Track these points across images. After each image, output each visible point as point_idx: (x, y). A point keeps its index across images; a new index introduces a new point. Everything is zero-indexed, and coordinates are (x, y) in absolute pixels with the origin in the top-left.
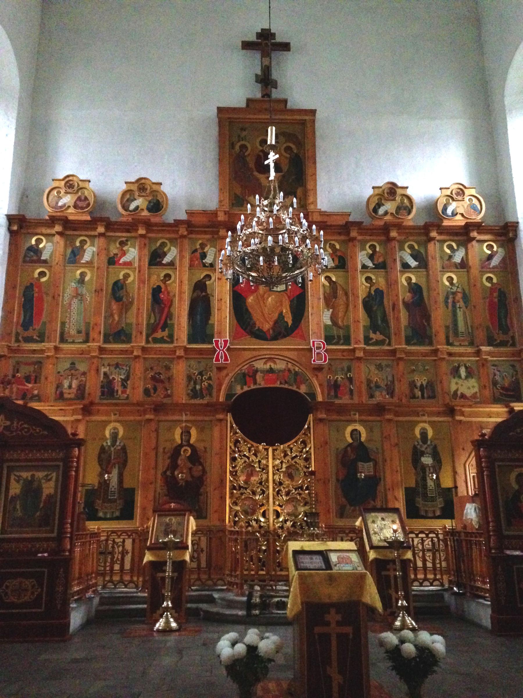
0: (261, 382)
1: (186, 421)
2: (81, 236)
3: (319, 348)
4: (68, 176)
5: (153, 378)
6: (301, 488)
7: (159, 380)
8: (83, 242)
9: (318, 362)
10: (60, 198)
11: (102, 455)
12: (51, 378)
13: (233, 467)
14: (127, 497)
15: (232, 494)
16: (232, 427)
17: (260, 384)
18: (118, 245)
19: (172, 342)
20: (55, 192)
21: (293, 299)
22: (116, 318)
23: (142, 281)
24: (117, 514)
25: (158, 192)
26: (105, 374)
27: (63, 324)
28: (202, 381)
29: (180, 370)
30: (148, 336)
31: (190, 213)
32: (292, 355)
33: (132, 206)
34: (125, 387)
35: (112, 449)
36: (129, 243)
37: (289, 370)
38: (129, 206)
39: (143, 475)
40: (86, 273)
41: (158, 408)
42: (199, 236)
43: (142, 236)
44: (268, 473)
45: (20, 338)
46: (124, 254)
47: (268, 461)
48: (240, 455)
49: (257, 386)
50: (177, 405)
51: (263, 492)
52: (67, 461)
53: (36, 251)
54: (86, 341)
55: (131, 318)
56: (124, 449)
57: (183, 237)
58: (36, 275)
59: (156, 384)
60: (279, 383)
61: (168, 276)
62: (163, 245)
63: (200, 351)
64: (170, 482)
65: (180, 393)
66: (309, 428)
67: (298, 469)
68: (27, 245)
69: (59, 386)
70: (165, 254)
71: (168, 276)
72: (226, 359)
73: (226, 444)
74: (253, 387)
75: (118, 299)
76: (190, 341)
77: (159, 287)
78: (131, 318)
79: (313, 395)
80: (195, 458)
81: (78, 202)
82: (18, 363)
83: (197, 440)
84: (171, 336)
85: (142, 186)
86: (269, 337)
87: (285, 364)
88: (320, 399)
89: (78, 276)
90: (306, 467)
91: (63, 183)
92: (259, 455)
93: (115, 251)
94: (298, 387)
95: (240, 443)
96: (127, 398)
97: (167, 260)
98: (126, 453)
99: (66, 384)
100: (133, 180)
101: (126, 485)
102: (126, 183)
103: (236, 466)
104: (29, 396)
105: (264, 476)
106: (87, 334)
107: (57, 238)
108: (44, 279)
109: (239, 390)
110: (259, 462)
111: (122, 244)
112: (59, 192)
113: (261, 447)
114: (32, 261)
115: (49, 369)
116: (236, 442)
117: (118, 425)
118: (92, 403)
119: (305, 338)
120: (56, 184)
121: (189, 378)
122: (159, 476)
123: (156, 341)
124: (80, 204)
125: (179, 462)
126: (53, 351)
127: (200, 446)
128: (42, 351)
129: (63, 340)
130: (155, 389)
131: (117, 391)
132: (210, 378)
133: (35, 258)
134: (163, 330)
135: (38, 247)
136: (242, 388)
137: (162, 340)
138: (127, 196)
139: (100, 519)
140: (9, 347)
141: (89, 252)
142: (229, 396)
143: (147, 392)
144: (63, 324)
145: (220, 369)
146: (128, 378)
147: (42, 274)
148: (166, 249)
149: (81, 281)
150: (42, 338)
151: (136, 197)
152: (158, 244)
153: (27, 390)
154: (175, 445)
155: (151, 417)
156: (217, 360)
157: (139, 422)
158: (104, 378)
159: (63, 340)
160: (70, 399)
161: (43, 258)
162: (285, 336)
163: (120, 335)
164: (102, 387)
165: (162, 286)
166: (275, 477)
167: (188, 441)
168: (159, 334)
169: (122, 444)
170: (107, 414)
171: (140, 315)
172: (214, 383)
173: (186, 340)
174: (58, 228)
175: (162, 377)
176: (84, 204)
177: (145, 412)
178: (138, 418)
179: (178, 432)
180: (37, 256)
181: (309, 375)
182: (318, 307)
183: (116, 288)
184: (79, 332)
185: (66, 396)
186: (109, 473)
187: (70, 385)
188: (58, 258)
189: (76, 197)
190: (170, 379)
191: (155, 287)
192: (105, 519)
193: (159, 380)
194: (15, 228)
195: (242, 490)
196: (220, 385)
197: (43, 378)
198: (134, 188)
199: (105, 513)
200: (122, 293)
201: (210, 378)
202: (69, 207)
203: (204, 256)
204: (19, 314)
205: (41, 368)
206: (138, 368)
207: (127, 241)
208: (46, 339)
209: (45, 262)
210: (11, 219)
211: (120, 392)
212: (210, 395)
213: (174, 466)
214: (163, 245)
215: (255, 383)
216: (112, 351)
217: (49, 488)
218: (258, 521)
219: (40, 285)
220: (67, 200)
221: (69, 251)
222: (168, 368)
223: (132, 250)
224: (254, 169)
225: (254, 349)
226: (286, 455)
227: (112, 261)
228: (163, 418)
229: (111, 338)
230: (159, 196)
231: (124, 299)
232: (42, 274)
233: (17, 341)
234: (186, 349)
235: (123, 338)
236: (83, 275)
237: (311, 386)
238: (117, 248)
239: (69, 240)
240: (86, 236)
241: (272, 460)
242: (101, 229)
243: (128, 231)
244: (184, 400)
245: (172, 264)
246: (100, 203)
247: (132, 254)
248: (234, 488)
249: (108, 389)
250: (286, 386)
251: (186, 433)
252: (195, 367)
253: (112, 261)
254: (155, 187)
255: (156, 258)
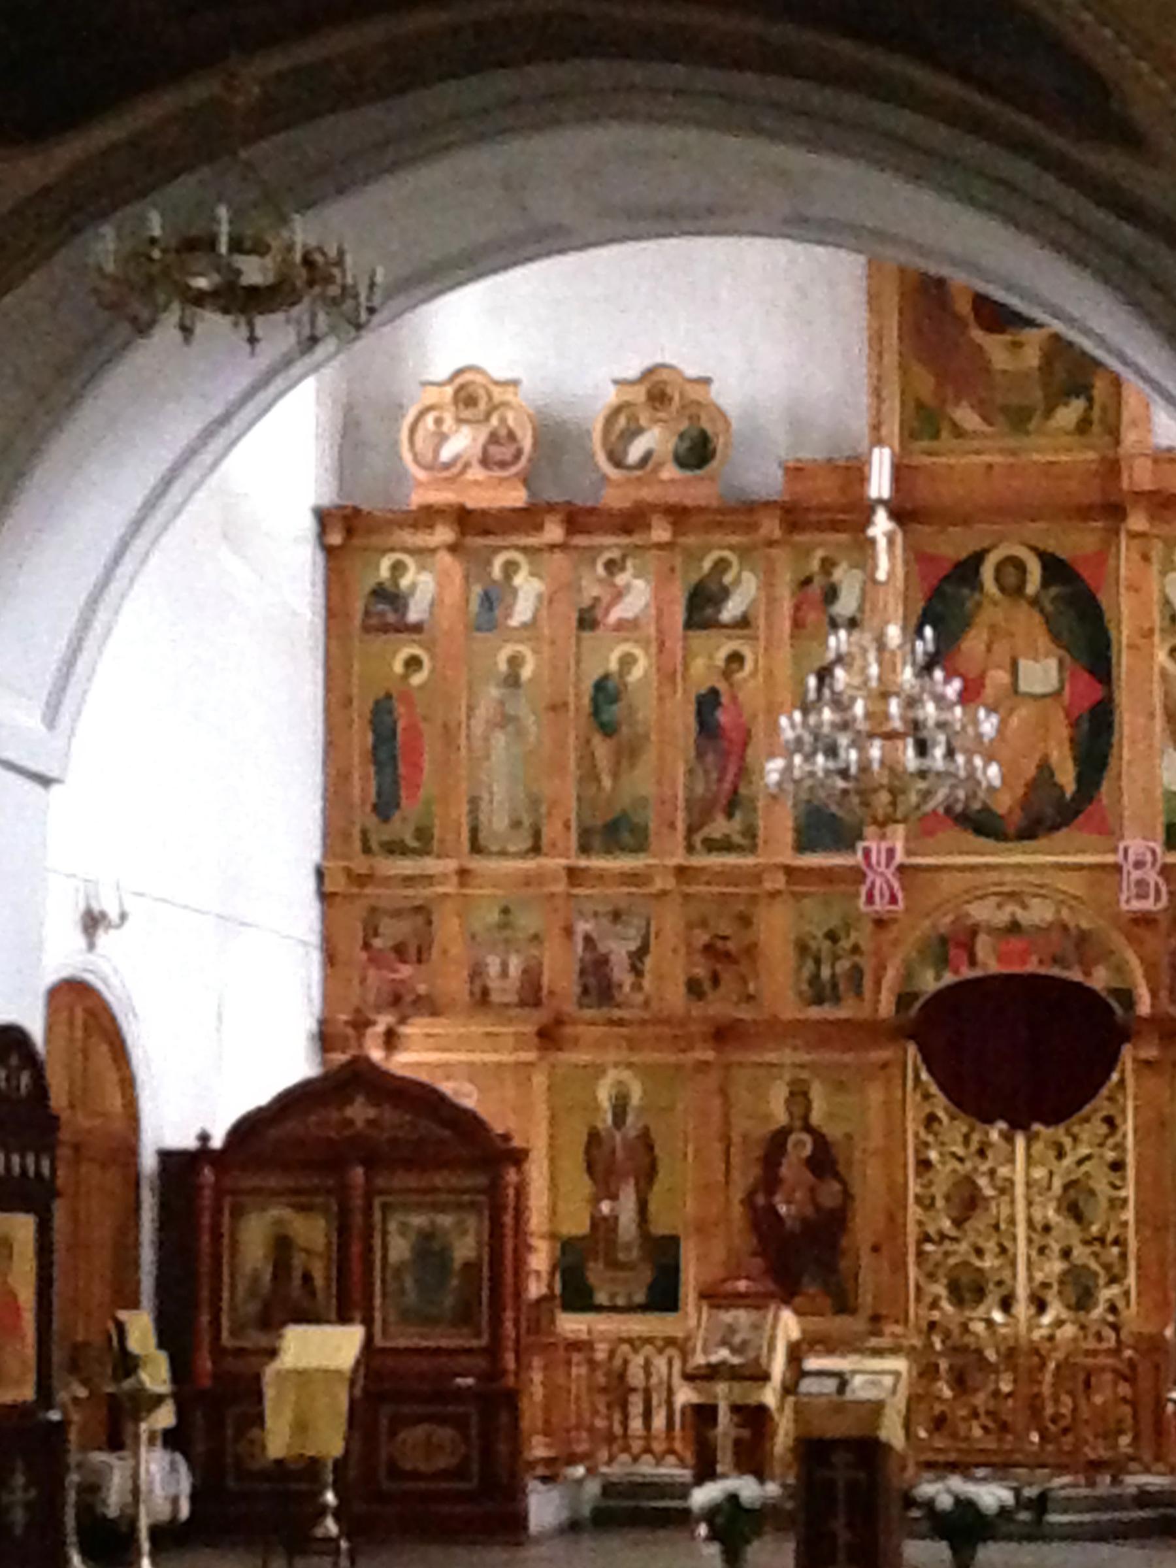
0: (990, 961)
1: (795, 1065)
2: (506, 548)
3: (1139, 865)
4: (459, 372)
5: (708, 949)
6: (1101, 1239)
7: (724, 958)
8: (510, 568)
9: (1136, 905)
10: (442, 438)
11: (595, 1152)
12: (455, 950)
13: (923, 1186)
14: (663, 1257)
15: (920, 1254)
16: (917, 1077)
17: (985, 965)
18: (600, 570)
19: (753, 849)
20: (430, 419)
21: (1079, 717)
22: (607, 782)
23: (667, 677)
24: (640, 1298)
25: (699, 403)
26: (588, 940)
27: (474, 802)
28: (836, 958)
29: (777, 928)
30: (691, 830)
31: (795, 471)
32: (1072, 884)
33: (635, 452)
34: (637, 972)
35: (618, 1137)
36: (629, 563)
37: (1065, 928)
38: (625, 452)
39: (697, 1202)
40: (523, 658)
41: (723, 1034)
42: (819, 537)
43: (660, 546)
44: (1012, 1202)
45: (374, 845)
46: (619, 595)
47: (1013, 1170)
48: (941, 1154)
49: (977, 973)
50: (774, 1021)
51: (1003, 1250)
52: (495, 1189)
53: (389, 597)
54: (536, 849)
55: (641, 782)
56: (646, 1140)
57: (771, 544)
58: (398, 667)
59: (719, 967)
60: (1034, 959)
61: (736, 658)
62: (721, 566)
63: (827, 876)
64: (763, 1220)
65: (779, 987)
66: (1122, 1082)
67: (1092, 1193)
68: (369, 584)
69: (477, 972)
70: (725, 593)
71: (736, 658)
72: (893, 900)
73: (902, 1131)
74: (968, 973)
75: (608, 730)
76: (801, 847)
77: (714, 692)
78: (641, 782)
79: (1126, 997)
80: (824, 1161)
81: (494, 450)
82: (373, 910)
83: (830, 1116)
84: (750, 832)
85: (657, 389)
86: (1011, 831)
87: (1053, 909)
88: (1144, 1007)
89: (503, 667)
90: (1115, 1187)
91: (449, 390)
92: (990, 1154)
93: (596, 591)
94: (1087, 974)
95: (940, 1121)
96: (646, 1004)
97: (731, 610)
98: (651, 1148)
99: (493, 966)
100: (633, 373)
101: (659, 1228)
102: (616, 382)
103: (930, 1183)
104: (409, 998)
105: (1005, 1211)
106: (537, 834)
107: (445, 558)
108: (417, 679)
109: (930, 982)
110: (992, 1173)
111: (612, 566)
112: (439, 421)
113: (994, 1136)
114: (385, 628)
115: (448, 928)
116: (931, 1120)
117: (626, 1075)
118: (559, 1022)
119: (1109, 832)
120: (431, 396)
121: (803, 948)
122: (737, 1210)
123: (712, 846)
124: (497, 452)
125: (784, 1171)
126: (455, 879)
127: (834, 1132)
128: (428, 879)
129: (476, 848)
130: (716, 980)
131: (620, 986)
132: (856, 949)
133: (391, 618)
134: (730, 815)
135: (397, 585)
136: (938, 977)
137: (725, 846)
138: (621, 425)
139: (599, 1309)
140: (348, 872)
141: (528, 591)
142: (904, 1000)
143: (694, 988)
144: (474, 811)
145: (880, 923)
146: (643, 951)
147: (413, 663)
148: (728, 579)
149: (512, 680)
150: (424, 842)
151: (643, 422)
152: (707, 565)
153: (402, 981)
154: (774, 1127)
155: (710, 1055)
156: (870, 899)
157: (678, 1067)
158: (585, 949)
159: (476, 848)
160: (507, 1005)
161: (413, 616)
162: (1055, 827)
163: (615, 831)
164: (582, 972)
165: (722, 686)
166: (1032, 1210)
167: (806, 1118)
168: (719, 827)
169: (640, 1125)
170: (600, 1044)
171: (665, 773)
172: (868, 964)
173: (789, 837)
174: (444, 534)
175: (731, 946)
176: (506, 452)
177: (690, 1047)
178: (672, 1058)
179: (778, 1095)
180: (396, 610)
181: (1118, 940)
182: (1148, 734)
183: (601, 697)
184: (516, 824)
185: (495, 997)
186: (614, 1197)
187: (504, 972)
188: (448, 620)
189: (483, 437)
190: (751, 950)
191: (703, 691)
192: (614, 1309)
193: (724, 958)
194: (336, 539)
195: (948, 1245)
196: (882, 967)
197: (435, 952)
198: (639, 395)
199: (613, 1296)
200: (614, 712)
201: (856, 949)
202: (467, 465)
203: (831, 594)
204: (364, 778)
205: (429, 923)
206: (670, 922)
207: (624, 558)
208: (435, 844)
209: (417, 628)
210: (323, 518)
211: (627, 988)
212: (859, 994)
213: (770, 1181)
214: (721, 566)
215: (973, 962)
216: (601, 877)
217: (465, 1249)
218: (990, 1323)
219: (407, 697)
220: (462, 442)
221: (477, 590)
222: (745, 921)
223: (639, 584)
224: (971, 318)
225: (973, 868)
226: (1061, 1155)
227: (587, 621)
228: (736, 1057)
229: (597, 842)
230: (704, 417)
231: (625, 730)
232: (413, 663)
233: (367, 850)
234: (789, 871)
235: (626, 837)
236: (515, 662)
237: (1120, 969)
238: (600, 581)
239: (477, 563)
240: (517, 548)
241: (1024, 1169)
242: (554, 532)
243: (627, 531)
244: (790, 1009)
245: (744, 622)
246: (554, 438)
247: (637, 596)
248: (927, 1238)
249: (597, 984)
250: (1055, 971)
251: (799, 1095)
252: (817, 918)
253: (587, 621)
254: (694, 393)
255: (703, 604)
